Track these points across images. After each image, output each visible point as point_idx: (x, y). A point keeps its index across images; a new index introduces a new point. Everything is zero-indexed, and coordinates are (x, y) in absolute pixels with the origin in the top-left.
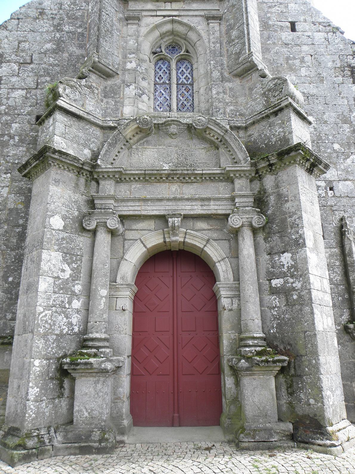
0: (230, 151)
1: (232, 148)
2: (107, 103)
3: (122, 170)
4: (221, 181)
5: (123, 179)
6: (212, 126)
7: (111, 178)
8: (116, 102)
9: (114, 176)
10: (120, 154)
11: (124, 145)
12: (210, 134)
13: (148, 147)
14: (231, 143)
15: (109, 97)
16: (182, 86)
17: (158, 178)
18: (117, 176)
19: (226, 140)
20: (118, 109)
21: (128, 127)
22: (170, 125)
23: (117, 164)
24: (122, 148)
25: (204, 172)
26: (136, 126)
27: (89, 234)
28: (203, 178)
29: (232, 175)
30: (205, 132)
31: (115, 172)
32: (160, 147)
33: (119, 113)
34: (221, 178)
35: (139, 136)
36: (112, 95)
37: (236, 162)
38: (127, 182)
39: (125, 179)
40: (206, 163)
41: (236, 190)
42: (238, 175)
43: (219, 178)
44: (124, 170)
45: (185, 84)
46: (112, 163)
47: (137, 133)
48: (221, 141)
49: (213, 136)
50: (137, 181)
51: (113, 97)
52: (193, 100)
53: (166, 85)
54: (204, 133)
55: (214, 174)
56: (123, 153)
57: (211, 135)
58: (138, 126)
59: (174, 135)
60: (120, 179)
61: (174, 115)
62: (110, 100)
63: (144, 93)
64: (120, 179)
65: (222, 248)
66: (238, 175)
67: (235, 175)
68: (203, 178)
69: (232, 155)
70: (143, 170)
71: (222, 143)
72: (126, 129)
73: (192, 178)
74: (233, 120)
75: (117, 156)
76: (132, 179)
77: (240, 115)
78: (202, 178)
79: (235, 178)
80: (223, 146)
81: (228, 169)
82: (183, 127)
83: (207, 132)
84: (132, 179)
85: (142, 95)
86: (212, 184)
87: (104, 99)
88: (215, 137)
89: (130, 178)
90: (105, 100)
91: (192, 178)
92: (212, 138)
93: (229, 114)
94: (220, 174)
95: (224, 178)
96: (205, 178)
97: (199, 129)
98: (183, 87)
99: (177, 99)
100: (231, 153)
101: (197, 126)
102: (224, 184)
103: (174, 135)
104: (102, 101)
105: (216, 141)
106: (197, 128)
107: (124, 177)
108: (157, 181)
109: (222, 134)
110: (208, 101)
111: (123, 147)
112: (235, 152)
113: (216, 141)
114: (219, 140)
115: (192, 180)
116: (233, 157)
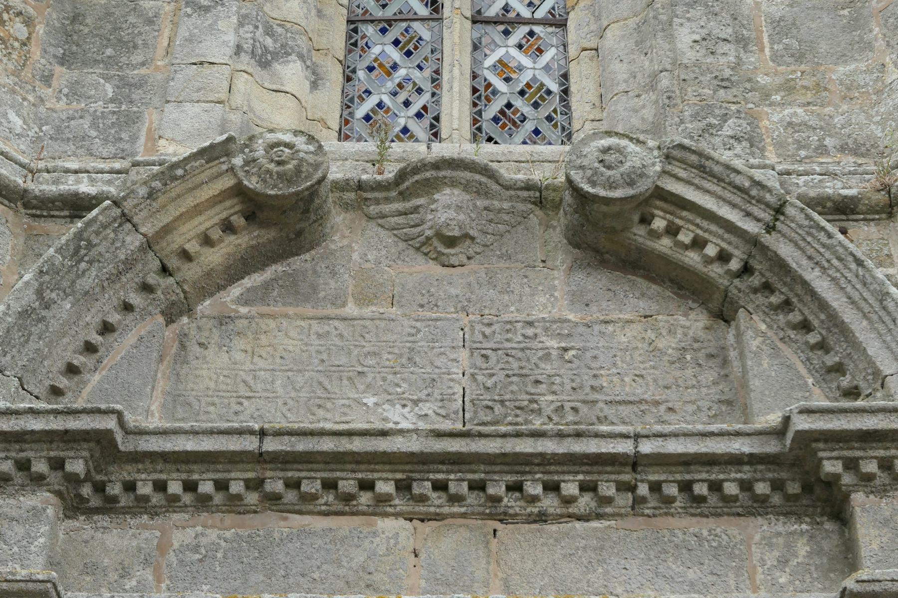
0: (805, 326)
1: (823, 305)
2: (75, 92)
3: (110, 423)
4: (759, 506)
5: (115, 489)
6: (688, 183)
7: (38, 480)
8: (124, 84)
9: (58, 464)
10: (110, 338)
11: (146, 288)
12: (672, 231)
13: (291, 311)
14: (812, 276)
15: (85, 64)
16: (501, 28)
17: (347, 485)
18: (77, 467)
19: (781, 265)
20: (131, 120)
21: (177, 188)
22: (430, 186)
23: (88, 391)
24: (127, 307)
25: (647, 447)
26: (228, 182)
27: (828, 474)
28: (643, 490)
29: (831, 467)
30: (646, 220)
31: (68, 437)
32: (368, 311)
33: (134, 139)
34: (761, 488)
35: (241, 242)
36: (109, 52)
37: (853, 393)
38: (142, 505)
39: (130, 487)
40: (657, 403)
41: (866, 562)
42: (871, 467)
43: (746, 486)
44: (127, 432)
45: (520, 21)
46: (56, 392)
47: (228, 227)
48: (746, 270)
49: (698, 244)
50: (204, 502)
51: (109, 62)
52: (566, 92)
53: (416, 25)
54: (640, 231)
55: (710, 461)
56: (131, 339)
57: (685, 237)
58: (239, 184)
59: (451, 242)
60: (99, 488)
61: (456, 143)
62: (93, 76)
63: (283, 52)
64: (99, 488)
65: (283, 197)
66: (871, 467)
67: (851, 465)
68: (643, 490)
69: (823, 346)
70: (252, 432)
71: (756, 280)
72: (162, 199)
73: (570, 488)
74: (807, 173)
75: (90, 348)
76: (175, 488)
77: (843, 149)
78: (632, 489)
79: (855, 487)
80: (760, 299)
81: (802, 423)
82: (506, 205)
83: (659, 224)
84: (175, 488)
85: (276, 56)
86: (704, 526)
87: (58, 69)
88: (711, 251)
89: (160, 486)
90: (62, 75)
91: (570, 488)
92: (692, 258)
93: (780, 145)
94: (753, 459)
95: (778, 485)
96: (656, 487)
97: (607, 201)
98: (506, 33)
99: (475, 90)
100: (813, 338)
101: (593, 184)
102: (781, 526)
103: (451, 242)
104: (47, 80)
105: (716, 271)
106: (595, 198)
107: (127, 473)
108: (340, 507)
109: (751, 227)
110: (652, 85)
111: (136, 299)
112: (844, 331)
113: (716, 271)
114: (735, 265)
115: (569, 501)
116: (831, 360)
